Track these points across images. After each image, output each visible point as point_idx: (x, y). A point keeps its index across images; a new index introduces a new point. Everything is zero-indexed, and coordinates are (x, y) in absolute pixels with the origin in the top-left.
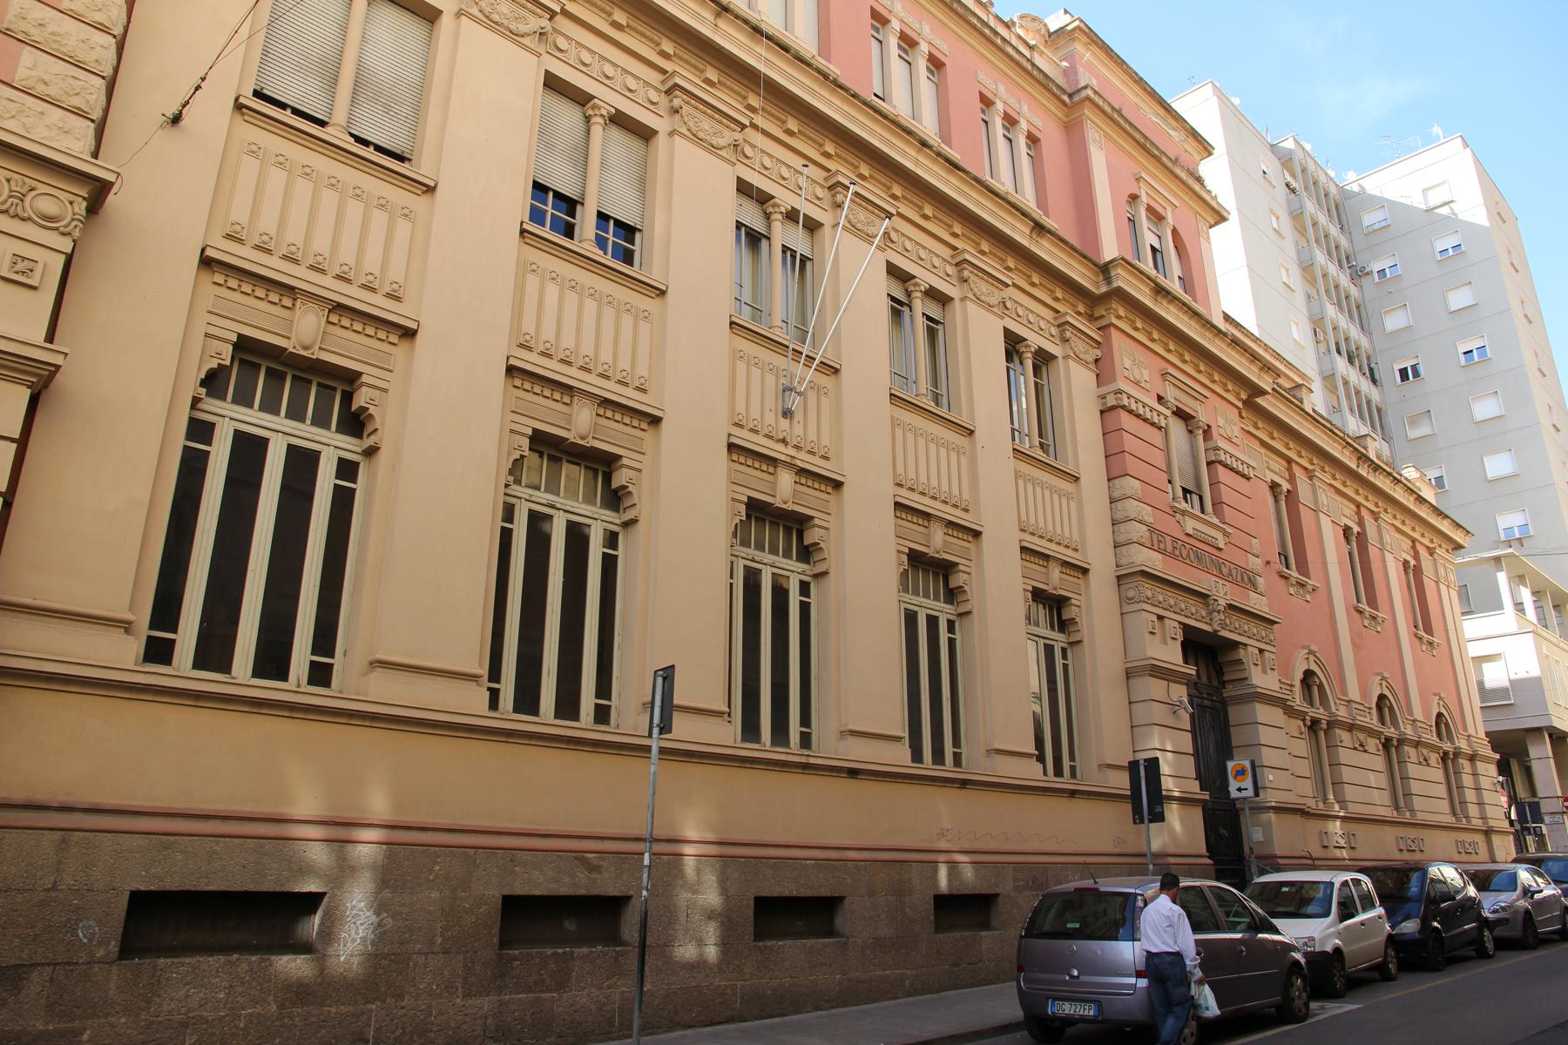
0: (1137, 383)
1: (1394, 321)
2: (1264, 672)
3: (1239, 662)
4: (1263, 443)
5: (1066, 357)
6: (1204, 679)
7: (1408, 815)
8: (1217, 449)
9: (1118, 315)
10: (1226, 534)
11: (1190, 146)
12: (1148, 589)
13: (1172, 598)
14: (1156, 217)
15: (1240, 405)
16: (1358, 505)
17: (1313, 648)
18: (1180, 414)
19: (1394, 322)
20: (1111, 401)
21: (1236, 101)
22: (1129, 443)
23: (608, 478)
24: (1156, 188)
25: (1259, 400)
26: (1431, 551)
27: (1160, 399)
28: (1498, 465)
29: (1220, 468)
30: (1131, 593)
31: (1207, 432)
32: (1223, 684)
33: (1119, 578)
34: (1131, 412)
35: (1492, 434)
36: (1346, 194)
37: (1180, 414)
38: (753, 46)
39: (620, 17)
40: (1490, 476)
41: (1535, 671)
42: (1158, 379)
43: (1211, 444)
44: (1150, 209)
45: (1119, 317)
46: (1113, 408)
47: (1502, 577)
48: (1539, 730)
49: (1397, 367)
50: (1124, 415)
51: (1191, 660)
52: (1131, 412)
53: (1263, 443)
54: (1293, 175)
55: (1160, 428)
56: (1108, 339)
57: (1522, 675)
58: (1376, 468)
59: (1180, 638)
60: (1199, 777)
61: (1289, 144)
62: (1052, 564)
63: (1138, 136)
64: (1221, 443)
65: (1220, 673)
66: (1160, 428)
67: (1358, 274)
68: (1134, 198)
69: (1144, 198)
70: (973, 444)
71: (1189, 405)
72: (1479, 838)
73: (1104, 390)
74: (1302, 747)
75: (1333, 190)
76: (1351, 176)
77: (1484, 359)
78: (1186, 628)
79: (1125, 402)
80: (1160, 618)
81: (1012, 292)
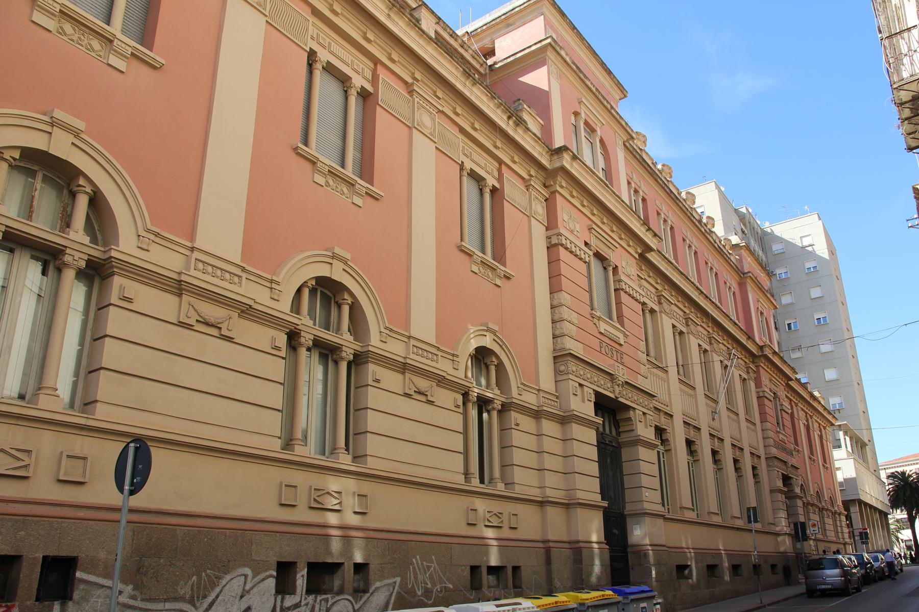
0: (572, 232)
1: (786, 300)
2: (646, 427)
3: (629, 419)
4: (462, 130)
5: (661, 312)
6: (607, 431)
7: (501, 486)
8: (559, 234)
9: (562, 186)
10: (626, 336)
11: (617, 94)
12: (776, 463)
13: (589, 373)
14: (591, 130)
15: (637, 256)
16: (806, 413)
17: (491, 325)
18: (598, 255)
19: (786, 300)
20: (761, 394)
21: (723, 189)
22: (564, 269)
23: (615, 416)
24: (591, 110)
25: (648, 255)
26: (825, 428)
27: (586, 244)
28: (830, 374)
29: (622, 293)
30: (562, 368)
31: (615, 269)
32: (619, 433)
33: (555, 358)
34: (566, 249)
35: (828, 360)
36: (764, 233)
37: (598, 255)
38: (408, 30)
39: (337, 7)
40: (827, 379)
41: (854, 475)
42: (587, 232)
43: (617, 278)
44: (586, 123)
45: (562, 187)
46: (556, 245)
47: (841, 433)
48: (854, 500)
49: (787, 322)
50: (561, 249)
51: (600, 412)
52: (566, 249)
53: (462, 130)
54: (745, 225)
55: (585, 262)
56: (758, 370)
57: (849, 476)
58: (829, 413)
59: (593, 399)
60: (602, 493)
61: (744, 210)
62: (662, 414)
63: (581, 76)
64: (623, 277)
65: (617, 426)
66: (585, 262)
67: (770, 274)
68: (576, 114)
69: (583, 115)
70: (695, 392)
71: (605, 251)
72: (842, 546)
73: (550, 233)
74: (277, 368)
75: (759, 231)
76: (767, 224)
77: (826, 324)
78: (597, 394)
79: (564, 242)
80: (581, 385)
81: (699, 328)
